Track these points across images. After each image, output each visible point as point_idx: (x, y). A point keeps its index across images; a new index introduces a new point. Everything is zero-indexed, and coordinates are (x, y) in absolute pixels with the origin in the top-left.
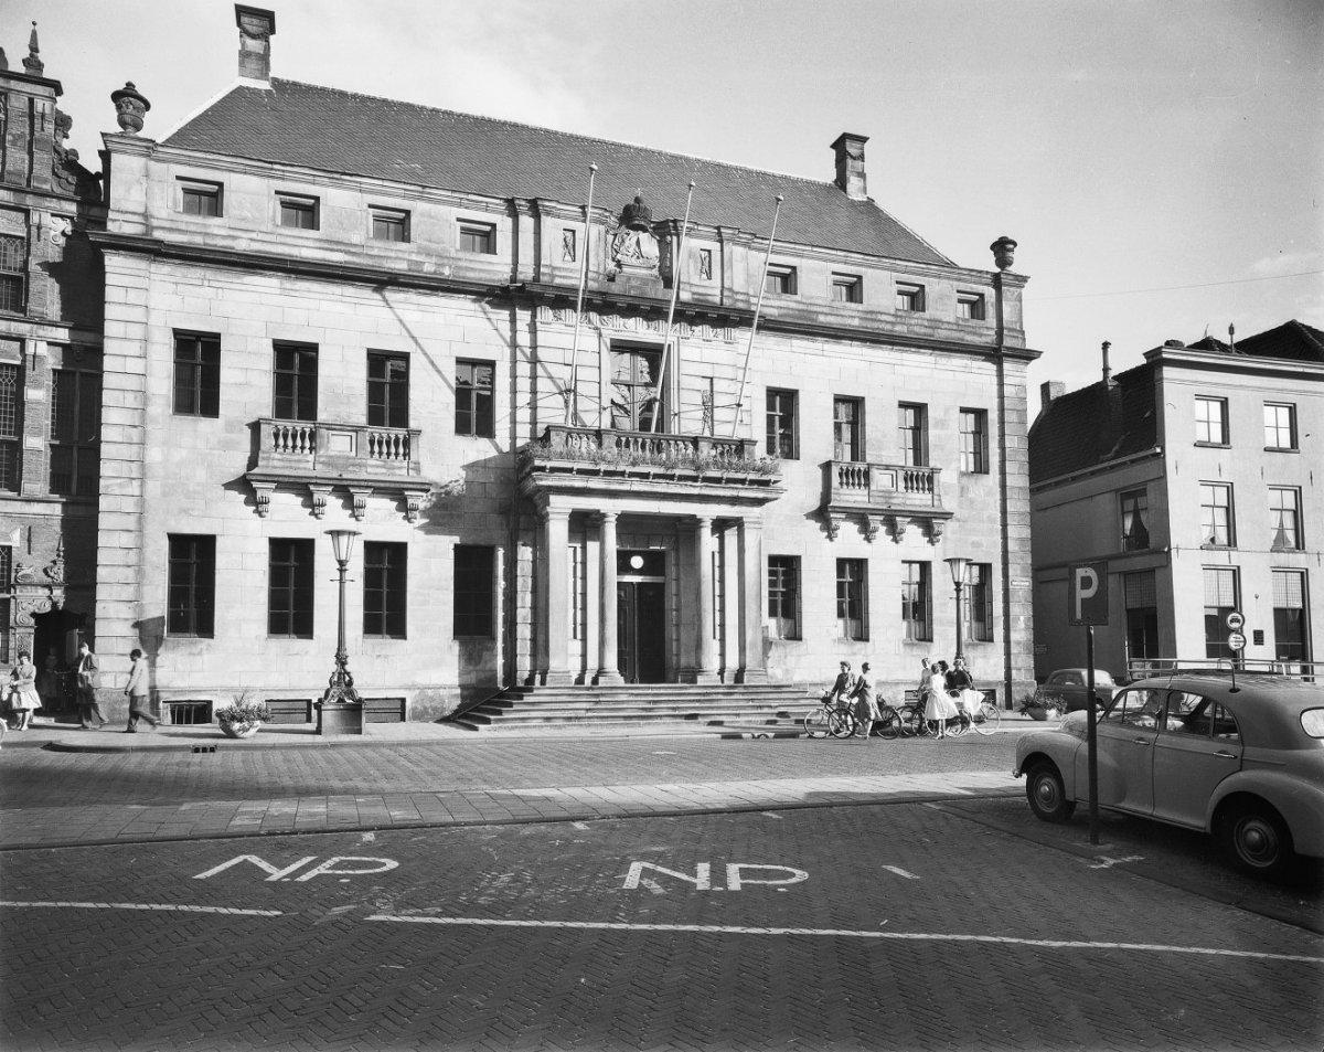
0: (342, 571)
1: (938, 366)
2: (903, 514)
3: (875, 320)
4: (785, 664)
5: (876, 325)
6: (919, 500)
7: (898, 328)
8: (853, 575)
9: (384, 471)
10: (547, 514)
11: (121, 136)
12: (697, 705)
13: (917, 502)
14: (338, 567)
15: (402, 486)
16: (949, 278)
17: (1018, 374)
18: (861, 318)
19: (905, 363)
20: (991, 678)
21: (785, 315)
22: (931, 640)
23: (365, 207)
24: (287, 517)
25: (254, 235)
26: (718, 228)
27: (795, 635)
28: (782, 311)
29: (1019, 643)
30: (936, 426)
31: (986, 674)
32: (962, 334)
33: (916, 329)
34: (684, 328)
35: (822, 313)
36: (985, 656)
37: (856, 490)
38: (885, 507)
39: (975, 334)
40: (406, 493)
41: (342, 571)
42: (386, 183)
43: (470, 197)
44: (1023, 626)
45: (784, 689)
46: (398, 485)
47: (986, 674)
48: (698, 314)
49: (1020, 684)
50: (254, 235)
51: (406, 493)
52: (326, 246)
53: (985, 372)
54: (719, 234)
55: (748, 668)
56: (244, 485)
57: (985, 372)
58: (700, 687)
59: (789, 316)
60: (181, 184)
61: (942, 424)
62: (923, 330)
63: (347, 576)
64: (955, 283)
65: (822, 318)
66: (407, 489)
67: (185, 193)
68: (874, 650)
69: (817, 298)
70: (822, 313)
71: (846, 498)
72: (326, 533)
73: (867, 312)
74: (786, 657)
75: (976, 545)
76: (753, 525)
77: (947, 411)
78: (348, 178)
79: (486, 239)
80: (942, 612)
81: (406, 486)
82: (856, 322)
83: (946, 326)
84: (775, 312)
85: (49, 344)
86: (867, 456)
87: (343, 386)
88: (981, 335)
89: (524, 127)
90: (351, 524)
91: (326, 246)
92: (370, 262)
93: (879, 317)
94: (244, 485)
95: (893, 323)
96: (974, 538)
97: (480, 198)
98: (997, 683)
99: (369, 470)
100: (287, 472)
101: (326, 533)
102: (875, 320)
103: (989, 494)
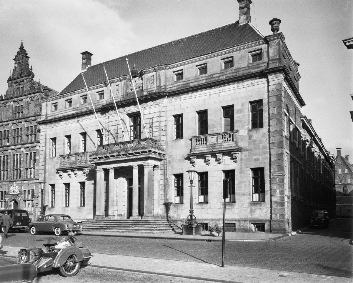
0: (191, 183)
1: (238, 88)
2: (219, 152)
3: (212, 78)
4: (177, 212)
5: (212, 80)
6: (228, 145)
7: (221, 78)
8: (204, 177)
9: (80, 164)
10: (96, 171)
11: (274, 35)
12: (117, 226)
13: (226, 146)
14: (190, 182)
15: (81, 167)
16: (244, 49)
17: (277, 79)
18: (206, 79)
19: (223, 91)
20: (263, 218)
21: (178, 88)
22: (235, 202)
23: (79, 97)
24: (200, 165)
25: (62, 112)
26: (154, 68)
27: (206, 202)
28: (178, 87)
29: (276, 202)
30: (237, 113)
31: (260, 216)
32: (250, 70)
33: (229, 75)
34: (144, 105)
35: (191, 83)
36: (260, 209)
37: (203, 146)
38: (211, 151)
39: (256, 68)
40: (232, 153)
41: (191, 183)
42: (82, 90)
43: (98, 85)
44: (279, 194)
45: (148, 221)
46: (202, 154)
47: (260, 216)
48: (144, 100)
49: (276, 221)
50: (62, 112)
51: (216, 155)
52: (73, 110)
53: (261, 83)
54: (155, 69)
55: (145, 214)
56: (188, 158)
57: (261, 83)
58: (130, 220)
59: (180, 88)
60: (197, 67)
61: (240, 111)
62: (234, 74)
63: (193, 185)
64: (248, 49)
65: (191, 85)
66: (232, 152)
67: (225, 64)
68: (210, 207)
69: (190, 77)
70: (191, 83)
71: (197, 149)
72: (187, 171)
73: (73, 109)
74: (178, 210)
75: (257, 160)
76: (99, 171)
77: (243, 105)
78: (75, 91)
79: (101, 94)
80: (240, 190)
81: (82, 167)
82: (204, 81)
83: (243, 69)
84: (175, 88)
85: (11, 150)
86: (208, 132)
87: (217, 122)
88: (259, 68)
89: (151, 48)
90: (193, 169)
91: (73, 110)
92: (80, 111)
93: (214, 76)
94: (188, 158)
95: (219, 77)
96: (256, 157)
97: (99, 85)
98: (266, 221)
99: (77, 164)
100: (63, 168)
101: (187, 171)
102: (212, 78)
103: (263, 136)
